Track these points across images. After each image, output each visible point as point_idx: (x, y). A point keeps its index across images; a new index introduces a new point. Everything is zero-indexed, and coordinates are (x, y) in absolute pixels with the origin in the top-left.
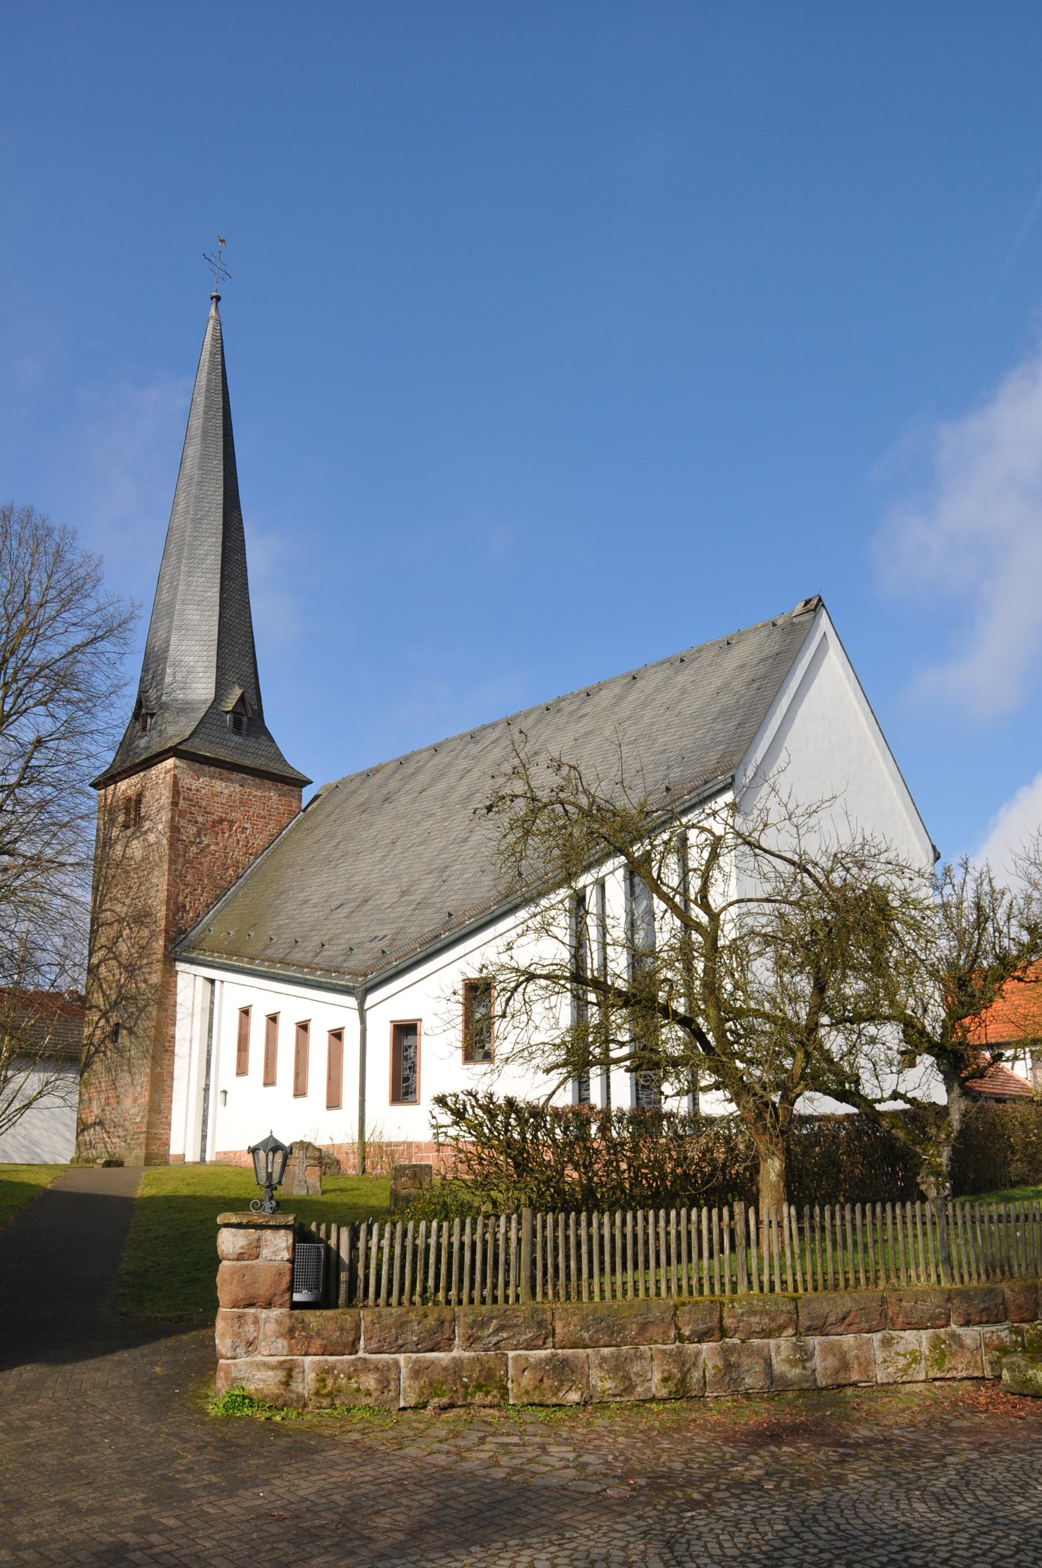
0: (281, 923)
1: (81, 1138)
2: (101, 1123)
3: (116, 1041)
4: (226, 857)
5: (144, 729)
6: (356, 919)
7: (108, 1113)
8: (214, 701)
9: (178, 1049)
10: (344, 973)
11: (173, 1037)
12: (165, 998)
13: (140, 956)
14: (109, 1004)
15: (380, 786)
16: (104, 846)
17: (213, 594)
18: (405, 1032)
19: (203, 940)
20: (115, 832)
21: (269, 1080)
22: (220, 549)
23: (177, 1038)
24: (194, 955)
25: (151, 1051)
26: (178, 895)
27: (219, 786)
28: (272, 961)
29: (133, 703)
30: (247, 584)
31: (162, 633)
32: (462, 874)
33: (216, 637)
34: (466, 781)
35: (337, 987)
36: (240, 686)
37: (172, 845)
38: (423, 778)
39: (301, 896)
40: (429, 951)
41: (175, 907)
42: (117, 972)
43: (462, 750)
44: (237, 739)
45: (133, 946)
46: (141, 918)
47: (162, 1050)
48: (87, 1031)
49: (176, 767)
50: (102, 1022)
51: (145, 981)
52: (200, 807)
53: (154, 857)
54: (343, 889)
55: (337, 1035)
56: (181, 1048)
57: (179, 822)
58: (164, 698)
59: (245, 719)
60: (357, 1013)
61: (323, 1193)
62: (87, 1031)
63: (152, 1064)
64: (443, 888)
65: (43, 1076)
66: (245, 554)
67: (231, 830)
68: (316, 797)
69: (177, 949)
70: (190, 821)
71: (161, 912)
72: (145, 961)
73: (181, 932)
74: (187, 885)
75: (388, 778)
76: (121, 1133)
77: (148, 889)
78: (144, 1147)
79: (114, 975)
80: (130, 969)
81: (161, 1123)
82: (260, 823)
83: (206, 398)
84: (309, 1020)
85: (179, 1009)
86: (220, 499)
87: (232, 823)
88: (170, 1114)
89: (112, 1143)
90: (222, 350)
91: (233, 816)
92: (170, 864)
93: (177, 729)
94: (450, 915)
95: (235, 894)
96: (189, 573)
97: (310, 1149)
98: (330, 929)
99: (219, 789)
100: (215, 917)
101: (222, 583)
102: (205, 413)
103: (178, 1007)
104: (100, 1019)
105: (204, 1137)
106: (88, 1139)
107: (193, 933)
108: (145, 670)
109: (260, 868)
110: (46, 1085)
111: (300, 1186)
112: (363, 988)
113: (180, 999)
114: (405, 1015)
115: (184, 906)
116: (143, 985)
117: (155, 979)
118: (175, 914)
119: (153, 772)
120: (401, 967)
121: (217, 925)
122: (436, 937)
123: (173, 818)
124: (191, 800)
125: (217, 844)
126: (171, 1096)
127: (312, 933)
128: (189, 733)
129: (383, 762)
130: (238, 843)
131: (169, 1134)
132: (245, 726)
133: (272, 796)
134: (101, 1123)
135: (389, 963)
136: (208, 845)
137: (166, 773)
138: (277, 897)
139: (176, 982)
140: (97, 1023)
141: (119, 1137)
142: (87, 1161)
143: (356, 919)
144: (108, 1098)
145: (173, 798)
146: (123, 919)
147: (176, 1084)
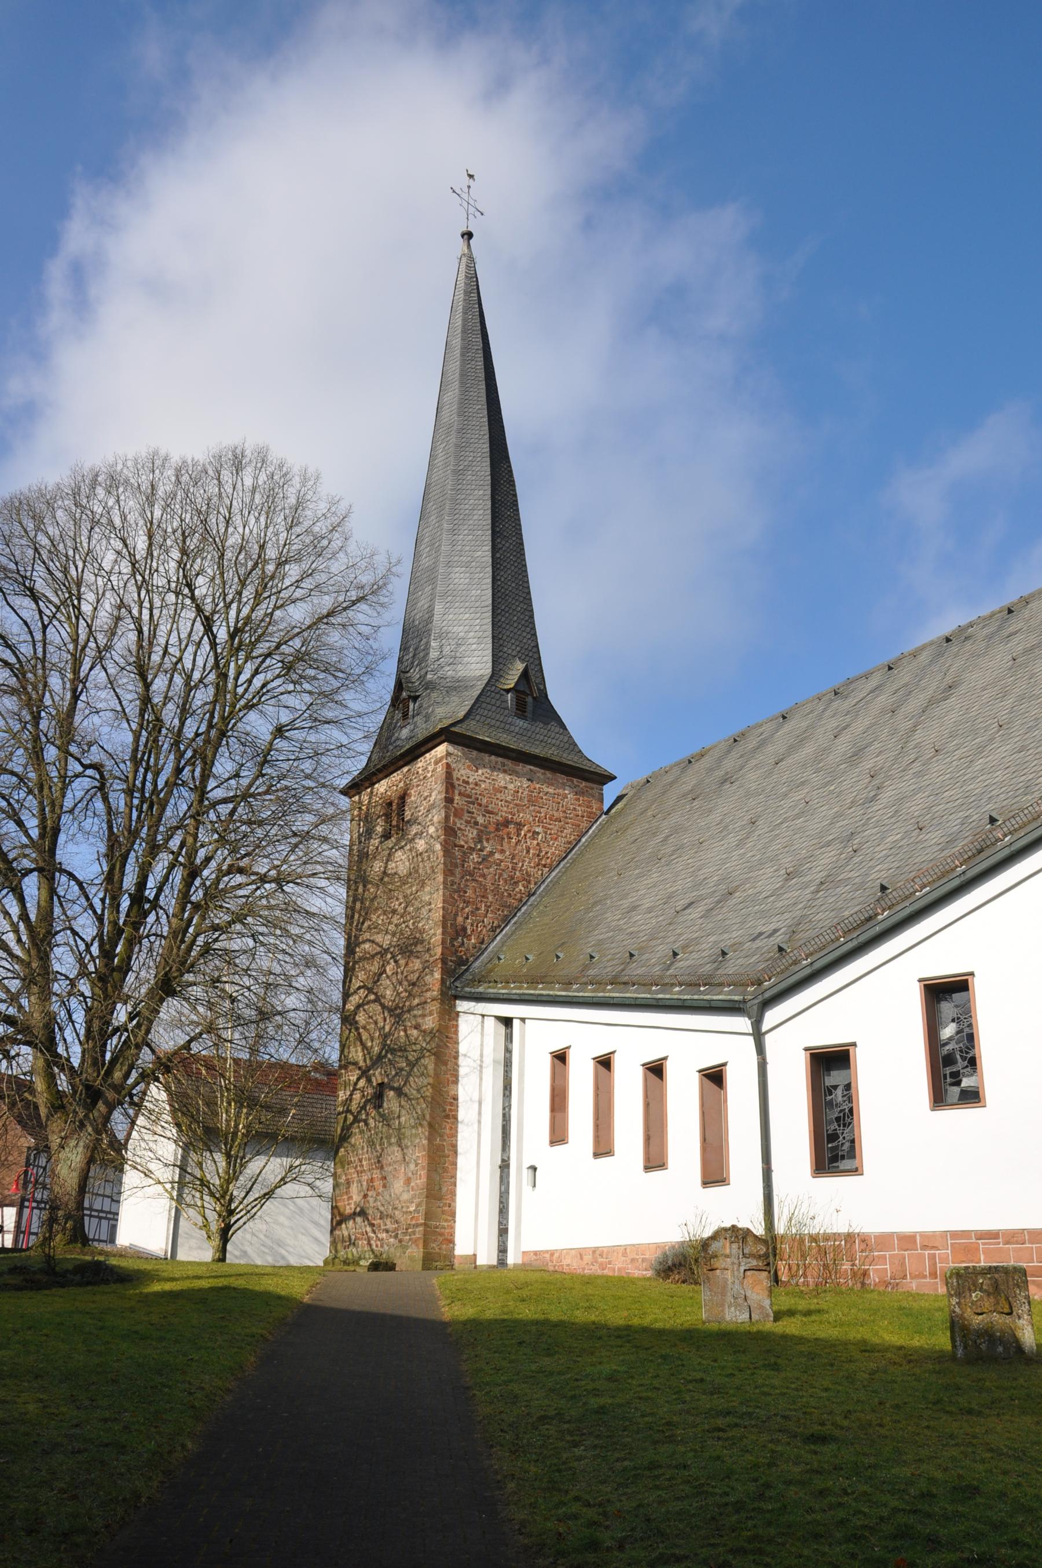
0: (601, 937)
1: (337, 1232)
2: (363, 1213)
3: (380, 1106)
4: (514, 869)
5: (405, 716)
6: (720, 917)
7: (371, 1200)
8: (491, 677)
9: (461, 1115)
10: (721, 985)
11: (456, 1099)
13: (410, 995)
14: (371, 1059)
15: (710, 770)
16: (360, 862)
17: (484, 553)
18: (830, 1063)
19: (491, 971)
21: (603, 1147)
22: (489, 503)
23: (460, 1100)
24: (481, 989)
25: (428, 1117)
26: (456, 915)
27: (502, 779)
30: (522, 544)
31: (423, 603)
32: (883, 838)
33: (490, 602)
35: (713, 1004)
36: (522, 661)
37: (447, 852)
38: (772, 750)
39: (626, 903)
41: (454, 932)
42: (380, 1018)
43: (825, 710)
44: (520, 723)
45: (400, 983)
46: (410, 946)
47: (441, 1115)
48: (342, 1095)
49: (448, 754)
50: (362, 1083)
51: (417, 1027)
52: (480, 805)
53: (424, 868)
54: (689, 885)
55: (715, 1077)
56: (465, 1112)
57: (455, 823)
58: (429, 676)
59: (529, 699)
60: (751, 1040)
61: (778, 1316)
62: (342, 1095)
63: (430, 1134)
64: (856, 860)
65: (286, 1161)
66: (518, 510)
67: (518, 835)
69: (457, 984)
70: (468, 822)
71: (435, 936)
72: (416, 1001)
74: (467, 903)
75: (720, 760)
76: (390, 1226)
77: (419, 909)
78: (421, 1245)
80: (397, 1013)
81: (443, 1212)
82: (555, 828)
83: (462, 339)
84: (665, 1058)
85: (461, 1061)
87: (519, 826)
88: (454, 1201)
89: (378, 1239)
90: (478, 288)
91: (521, 817)
92: (445, 875)
93: (446, 710)
94: (883, 888)
95: (528, 914)
96: (453, 532)
97: (750, 1239)
98: (680, 935)
99: (502, 784)
100: (503, 943)
101: (493, 541)
102: (463, 355)
103: (461, 1059)
104: (358, 1079)
105: (503, 1232)
106: (346, 1233)
107: (477, 964)
108: (404, 648)
109: (557, 882)
110: (290, 1171)
112: (760, 999)
113: (462, 1048)
114: (828, 1038)
115: (464, 929)
116: (415, 1032)
117: (430, 1023)
118: (453, 939)
119: (420, 765)
120: (818, 965)
121: (509, 950)
122: (869, 919)
123: (447, 818)
124: (469, 797)
125: (502, 851)
126: (454, 1177)
127: (653, 943)
128: (461, 714)
130: (528, 852)
131: (453, 1228)
132: (530, 708)
133: (565, 796)
134: (363, 1213)
135: (795, 962)
136: (492, 854)
137: (436, 763)
138: (588, 910)
139: (457, 1026)
140: (356, 1084)
141: (387, 1231)
142: (346, 1262)
143: (720, 917)
144: (372, 1180)
145: (447, 792)
146: (387, 950)
147: (461, 1161)
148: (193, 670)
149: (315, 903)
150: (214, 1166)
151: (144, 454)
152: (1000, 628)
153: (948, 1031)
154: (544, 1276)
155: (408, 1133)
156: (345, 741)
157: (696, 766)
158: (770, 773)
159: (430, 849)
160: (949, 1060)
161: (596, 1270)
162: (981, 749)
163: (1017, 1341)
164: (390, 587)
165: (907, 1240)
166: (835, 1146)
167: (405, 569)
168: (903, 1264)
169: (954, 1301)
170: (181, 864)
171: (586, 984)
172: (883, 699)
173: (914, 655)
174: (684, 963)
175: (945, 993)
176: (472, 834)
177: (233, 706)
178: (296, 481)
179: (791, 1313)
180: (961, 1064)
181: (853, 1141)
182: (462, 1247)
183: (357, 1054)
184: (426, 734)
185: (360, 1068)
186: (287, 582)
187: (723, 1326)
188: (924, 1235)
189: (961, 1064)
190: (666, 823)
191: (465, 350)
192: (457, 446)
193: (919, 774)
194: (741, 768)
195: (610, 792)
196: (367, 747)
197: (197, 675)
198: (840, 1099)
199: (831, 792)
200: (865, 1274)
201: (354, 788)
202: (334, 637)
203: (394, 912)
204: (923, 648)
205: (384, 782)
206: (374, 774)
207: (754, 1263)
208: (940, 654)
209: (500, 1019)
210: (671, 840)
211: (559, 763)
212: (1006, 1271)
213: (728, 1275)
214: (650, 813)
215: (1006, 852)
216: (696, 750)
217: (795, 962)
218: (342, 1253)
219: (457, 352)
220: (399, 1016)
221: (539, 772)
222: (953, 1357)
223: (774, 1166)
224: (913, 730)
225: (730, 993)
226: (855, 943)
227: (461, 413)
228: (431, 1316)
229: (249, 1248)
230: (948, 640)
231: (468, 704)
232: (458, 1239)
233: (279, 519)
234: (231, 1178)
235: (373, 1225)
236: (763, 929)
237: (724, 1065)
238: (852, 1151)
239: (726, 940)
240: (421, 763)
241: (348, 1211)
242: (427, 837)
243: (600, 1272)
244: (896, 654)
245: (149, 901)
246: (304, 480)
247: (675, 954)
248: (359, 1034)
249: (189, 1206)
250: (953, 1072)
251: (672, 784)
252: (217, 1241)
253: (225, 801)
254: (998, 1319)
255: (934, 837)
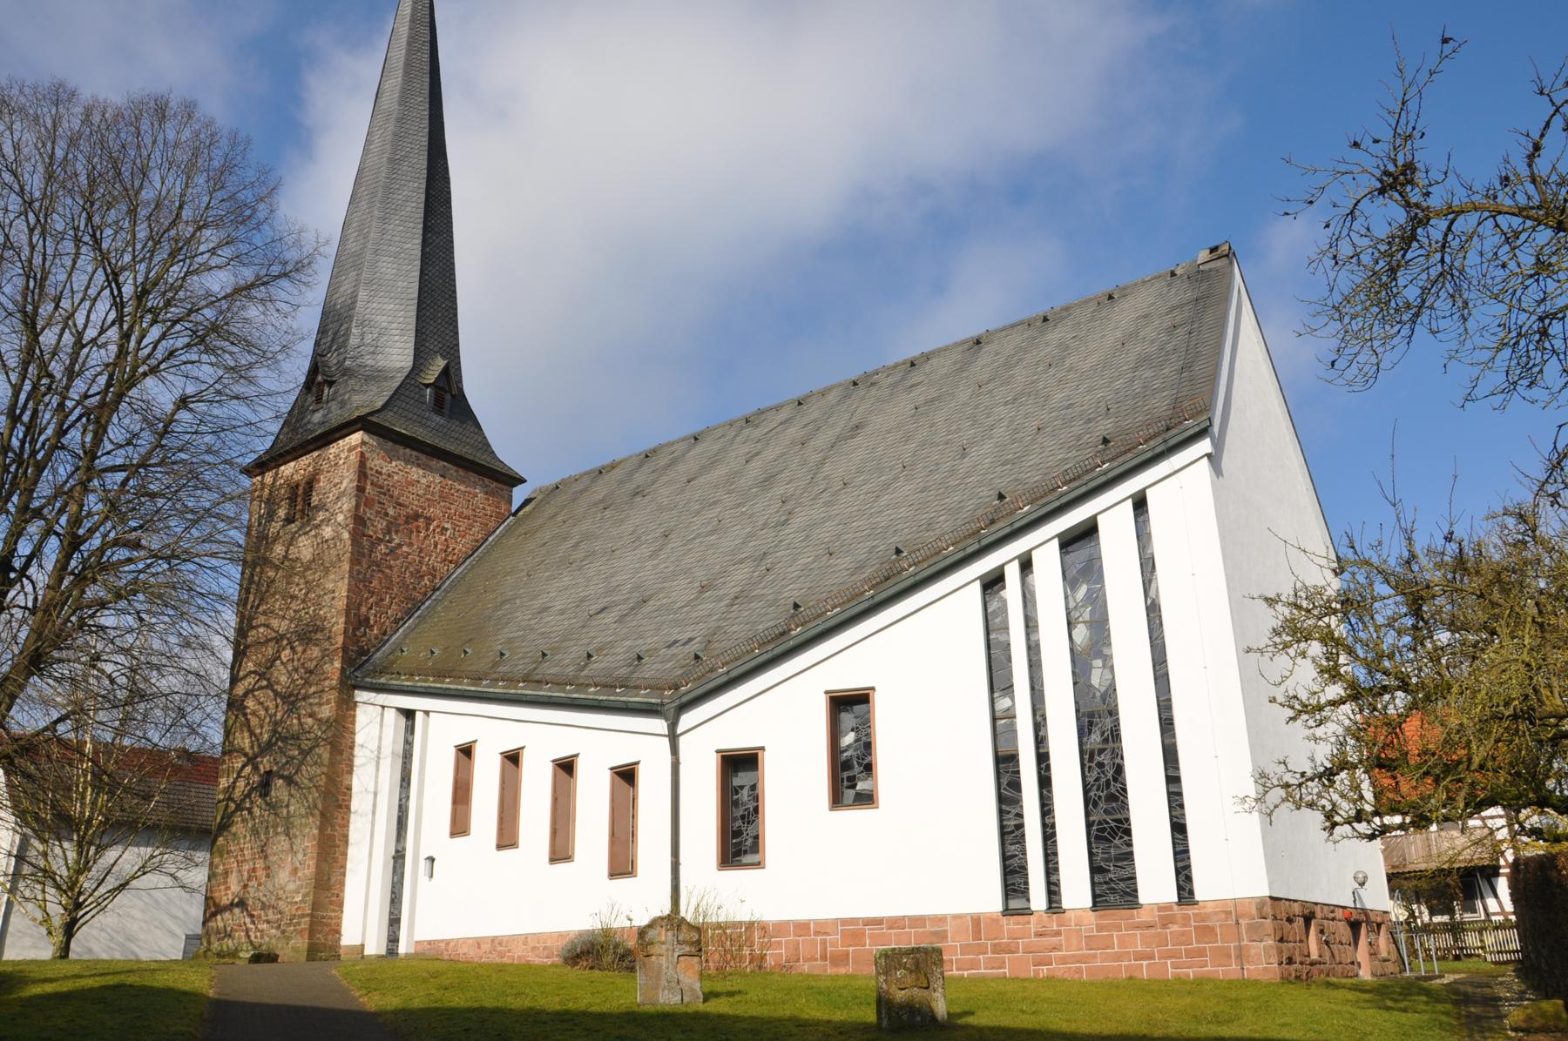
2: (242, 904)
5: (319, 400)
9: (354, 805)
10: (637, 687)
11: (349, 789)
12: (339, 737)
15: (621, 482)
18: (739, 766)
20: (275, 527)
22: (423, 197)
23: (354, 790)
24: (383, 680)
26: (360, 605)
27: (415, 473)
28: (510, 680)
29: (306, 365)
31: (346, 288)
33: (416, 295)
34: (756, 464)
36: (444, 358)
39: (537, 604)
40: (777, 651)
41: (357, 621)
42: (271, 705)
44: (438, 419)
45: (296, 670)
46: (309, 633)
47: (333, 805)
48: (224, 783)
49: (363, 443)
50: (248, 769)
56: (359, 802)
58: (347, 363)
59: (448, 397)
61: (708, 997)
64: (769, 578)
68: (527, 502)
71: (338, 625)
72: (313, 689)
73: (363, 652)
75: (631, 474)
76: (271, 917)
79: (267, 709)
81: (331, 903)
82: (463, 525)
85: (357, 751)
86: (425, 141)
87: (429, 520)
94: (796, 606)
96: (384, 220)
97: (684, 927)
100: (405, 636)
102: (409, 44)
104: (243, 767)
105: (394, 922)
107: (378, 655)
108: (322, 330)
111: (670, 989)
112: (677, 703)
113: (359, 738)
114: (739, 741)
115: (368, 619)
116: (310, 721)
117: (326, 712)
118: (355, 630)
120: (734, 674)
121: (412, 643)
122: (783, 634)
123: (357, 507)
124: (381, 487)
125: (411, 545)
126: (344, 867)
128: (379, 404)
129: (618, 458)
131: (340, 918)
132: (447, 404)
133: (477, 496)
134: (242, 904)
135: (712, 670)
136: (399, 546)
137: (350, 450)
138: (496, 609)
142: (220, 955)
144: (254, 870)
146: (282, 637)
148: (85, 326)
149: (206, 582)
150: (62, 856)
151: (47, 84)
152: (903, 379)
153: (848, 739)
154: (438, 962)
155: (297, 822)
156: (254, 419)
157: (606, 477)
158: (682, 491)
159: (337, 537)
160: (847, 765)
161: (495, 958)
162: (886, 486)
163: (932, 1011)
164: (315, 266)
165: (802, 927)
166: (739, 841)
167: (331, 250)
168: (797, 948)
169: (882, 979)
170: (1433, 642)
171: (497, 680)
172: (793, 432)
173: (823, 394)
174: (598, 665)
175: (848, 705)
176: (381, 525)
177: (135, 368)
178: (224, 143)
179: (717, 995)
180: (857, 769)
181: (756, 837)
182: (350, 936)
183: (243, 740)
184: (341, 420)
185: (246, 755)
186: (202, 248)
187: (659, 1008)
188: (817, 922)
189: (857, 769)
190: (576, 529)
191: (412, 40)
192: (395, 134)
193: (828, 504)
194: (653, 483)
195: (519, 494)
196: (275, 427)
197: (91, 333)
198: (745, 798)
199: (743, 513)
200: (763, 957)
201: (261, 466)
202: (253, 312)
203: (293, 597)
204: (831, 389)
205: (292, 464)
206: (281, 455)
207: (688, 949)
208: (846, 396)
209: (400, 710)
210: (582, 546)
211: (473, 462)
212: (925, 951)
213: (663, 960)
214: (559, 518)
215: (911, 581)
216: (607, 461)
217: (712, 670)
218: (215, 946)
219: (404, 41)
220: (293, 703)
221: (452, 469)
222: (878, 1027)
223: (682, 860)
224: (823, 462)
225: (646, 696)
226: (770, 655)
227: (403, 101)
228: (354, 1007)
229: (100, 940)
230: (855, 384)
231: (386, 395)
232: (344, 930)
233: (201, 180)
234: (83, 867)
235: (252, 916)
236: (678, 637)
237: (637, 763)
238: (756, 845)
239: (642, 646)
240: (333, 450)
241: (225, 901)
242: (335, 524)
243: (498, 960)
244: (806, 391)
245: (14, 570)
246: (234, 144)
247: (589, 656)
248: (248, 721)
249: (27, 899)
250: (851, 777)
251: (582, 491)
252: (59, 937)
253: (114, 469)
254: (917, 993)
255: (843, 562)
